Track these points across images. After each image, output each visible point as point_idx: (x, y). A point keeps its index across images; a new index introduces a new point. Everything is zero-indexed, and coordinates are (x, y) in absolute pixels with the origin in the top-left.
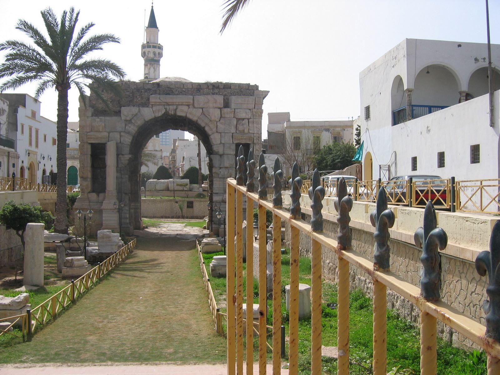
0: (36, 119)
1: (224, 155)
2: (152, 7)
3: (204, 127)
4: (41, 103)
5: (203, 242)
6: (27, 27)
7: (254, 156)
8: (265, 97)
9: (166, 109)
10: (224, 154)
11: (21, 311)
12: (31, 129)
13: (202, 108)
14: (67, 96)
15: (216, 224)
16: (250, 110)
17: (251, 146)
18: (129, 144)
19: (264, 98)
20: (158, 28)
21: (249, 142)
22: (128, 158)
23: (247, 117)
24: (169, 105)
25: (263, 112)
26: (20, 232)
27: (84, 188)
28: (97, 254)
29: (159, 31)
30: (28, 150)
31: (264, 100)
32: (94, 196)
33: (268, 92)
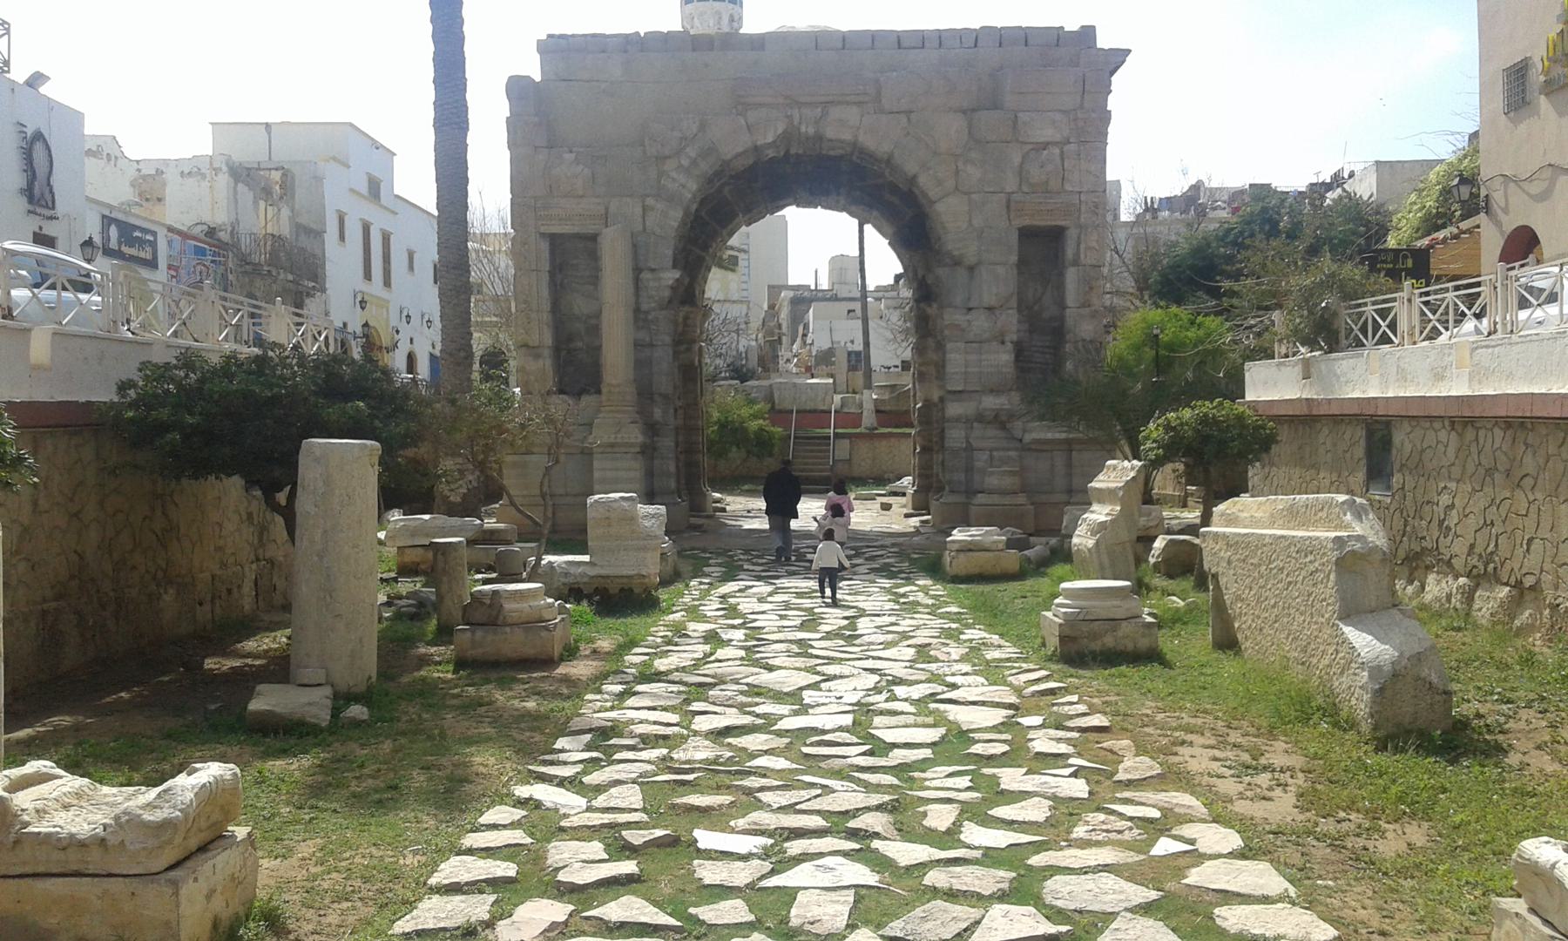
3: (915, 177)
4: (395, 154)
5: (953, 541)
7: (1071, 276)
8: (1118, 67)
9: (790, 117)
10: (979, 263)
11: (175, 884)
14: (465, 90)
15: (958, 492)
16: (1064, 112)
17: (1072, 234)
19: (1113, 73)
23: (1058, 138)
24: (800, 105)
25: (1110, 119)
26: (282, 497)
27: (532, 378)
28: (585, 580)
31: (1113, 78)
32: (560, 405)
33: (1129, 51)
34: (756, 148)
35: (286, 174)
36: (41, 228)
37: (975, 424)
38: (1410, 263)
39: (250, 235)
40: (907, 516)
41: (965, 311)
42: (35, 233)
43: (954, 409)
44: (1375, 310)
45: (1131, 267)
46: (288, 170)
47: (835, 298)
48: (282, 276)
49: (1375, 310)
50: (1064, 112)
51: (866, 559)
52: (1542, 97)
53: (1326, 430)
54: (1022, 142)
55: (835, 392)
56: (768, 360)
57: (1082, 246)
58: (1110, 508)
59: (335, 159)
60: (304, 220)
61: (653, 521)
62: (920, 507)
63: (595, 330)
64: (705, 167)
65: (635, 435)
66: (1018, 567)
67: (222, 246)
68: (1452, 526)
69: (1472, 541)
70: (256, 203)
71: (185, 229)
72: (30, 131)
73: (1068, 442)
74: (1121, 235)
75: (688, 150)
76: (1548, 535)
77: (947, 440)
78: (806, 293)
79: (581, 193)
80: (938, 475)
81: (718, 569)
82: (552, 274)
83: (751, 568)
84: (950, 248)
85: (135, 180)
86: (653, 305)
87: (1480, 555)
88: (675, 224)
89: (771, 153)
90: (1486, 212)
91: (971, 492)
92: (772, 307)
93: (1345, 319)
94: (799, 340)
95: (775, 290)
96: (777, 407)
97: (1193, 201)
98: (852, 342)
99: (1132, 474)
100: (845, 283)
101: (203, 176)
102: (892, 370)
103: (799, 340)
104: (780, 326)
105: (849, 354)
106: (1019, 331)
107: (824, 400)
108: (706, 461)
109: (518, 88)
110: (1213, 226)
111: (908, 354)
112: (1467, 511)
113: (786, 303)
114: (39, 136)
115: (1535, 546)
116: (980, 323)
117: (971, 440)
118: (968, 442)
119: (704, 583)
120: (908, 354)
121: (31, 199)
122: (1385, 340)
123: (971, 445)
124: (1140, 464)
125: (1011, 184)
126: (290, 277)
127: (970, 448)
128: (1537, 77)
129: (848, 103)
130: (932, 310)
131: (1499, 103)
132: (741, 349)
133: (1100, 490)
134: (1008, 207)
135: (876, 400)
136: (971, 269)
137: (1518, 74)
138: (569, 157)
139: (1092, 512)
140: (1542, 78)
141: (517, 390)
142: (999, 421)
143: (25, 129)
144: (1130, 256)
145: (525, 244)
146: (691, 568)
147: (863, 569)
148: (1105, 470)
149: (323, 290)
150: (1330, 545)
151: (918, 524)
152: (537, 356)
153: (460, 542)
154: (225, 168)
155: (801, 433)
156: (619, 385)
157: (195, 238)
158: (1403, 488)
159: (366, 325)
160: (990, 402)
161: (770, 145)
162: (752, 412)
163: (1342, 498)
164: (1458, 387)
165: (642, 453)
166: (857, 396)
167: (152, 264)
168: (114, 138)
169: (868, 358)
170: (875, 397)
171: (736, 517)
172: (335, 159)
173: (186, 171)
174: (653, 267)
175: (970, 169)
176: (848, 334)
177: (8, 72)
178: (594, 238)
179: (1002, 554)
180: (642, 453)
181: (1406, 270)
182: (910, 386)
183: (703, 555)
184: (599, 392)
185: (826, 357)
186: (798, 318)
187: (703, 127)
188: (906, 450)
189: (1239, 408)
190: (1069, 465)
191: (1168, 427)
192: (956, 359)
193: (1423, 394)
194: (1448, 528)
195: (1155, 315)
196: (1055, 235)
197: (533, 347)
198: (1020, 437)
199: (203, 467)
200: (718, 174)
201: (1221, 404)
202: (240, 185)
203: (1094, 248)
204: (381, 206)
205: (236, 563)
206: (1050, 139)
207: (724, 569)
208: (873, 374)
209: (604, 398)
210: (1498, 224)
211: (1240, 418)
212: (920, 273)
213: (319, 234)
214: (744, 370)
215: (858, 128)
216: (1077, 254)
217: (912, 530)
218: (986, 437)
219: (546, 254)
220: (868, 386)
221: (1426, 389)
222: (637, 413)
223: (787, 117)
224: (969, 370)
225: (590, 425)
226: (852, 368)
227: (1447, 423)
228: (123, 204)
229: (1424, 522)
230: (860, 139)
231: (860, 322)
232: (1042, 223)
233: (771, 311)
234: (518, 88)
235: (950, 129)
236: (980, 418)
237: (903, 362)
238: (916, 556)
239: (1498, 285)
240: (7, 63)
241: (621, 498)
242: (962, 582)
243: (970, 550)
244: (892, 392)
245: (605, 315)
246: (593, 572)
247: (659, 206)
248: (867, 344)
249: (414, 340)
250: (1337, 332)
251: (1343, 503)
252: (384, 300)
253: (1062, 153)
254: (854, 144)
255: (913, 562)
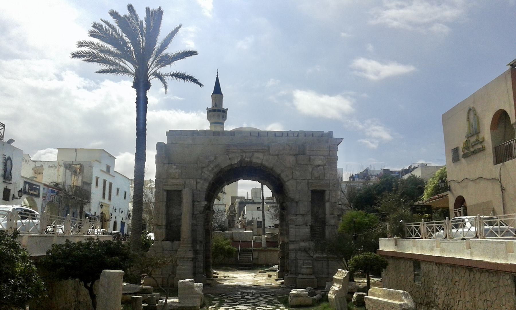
0: (111, 173)
1: (300, 202)
2: (217, 76)
5: (291, 294)
6: (114, 14)
7: (327, 205)
9: (242, 156)
12: (105, 182)
13: (278, 155)
16: (324, 156)
17: (327, 192)
18: (205, 190)
20: (222, 94)
21: (324, 189)
22: (204, 205)
23: (322, 163)
24: (245, 152)
26: (89, 285)
29: (223, 96)
30: (101, 202)
33: (343, 139)
34: (231, 165)
35: (82, 166)
36: (6, 187)
37: (298, 252)
38: (426, 209)
39: (69, 186)
40: (277, 280)
41: (295, 216)
42: (4, 188)
43: (291, 247)
44: (415, 226)
45: (347, 197)
46: (82, 165)
47: (253, 203)
48: (78, 199)
49: (415, 226)
50: (324, 156)
51: (264, 298)
52: (463, 159)
53: (402, 262)
54: (312, 165)
55: (253, 235)
56: (231, 224)
57: (331, 196)
58: (339, 285)
59: (97, 160)
60: (85, 180)
61: (199, 288)
62: (280, 277)
63: (179, 220)
64: (216, 170)
65: (191, 254)
66: (312, 303)
67: (60, 190)
68: (438, 295)
69: (443, 300)
70: (71, 175)
71: (48, 184)
72: (7, 157)
73: (327, 258)
74: (343, 186)
75: (211, 165)
76: (463, 300)
77: (289, 257)
78: (244, 200)
79: (177, 178)
80: (286, 266)
81: (217, 302)
82: (167, 202)
83: (228, 301)
84: (291, 196)
85: (34, 168)
86: (198, 212)
87: (446, 305)
88: (206, 188)
89: (236, 166)
90: (450, 191)
91: (297, 274)
92: (232, 204)
93: (406, 228)
94: (241, 216)
95: (234, 198)
96: (234, 240)
97: (365, 175)
98: (259, 218)
99: (345, 275)
100: (256, 197)
101: (56, 167)
102: (272, 227)
103: (241, 216)
104: (235, 211)
105: (258, 222)
106: (312, 222)
107: (249, 238)
108: (211, 261)
109: (160, 146)
110: (372, 184)
111: (278, 222)
112: (442, 290)
113: (237, 203)
114: (9, 158)
115: (460, 303)
116: (300, 220)
117: (297, 257)
118: (296, 257)
119: (213, 308)
120: (278, 222)
121: (4, 178)
122: (417, 236)
123: (297, 259)
124: (348, 272)
125: (309, 177)
126: (80, 199)
127: (296, 259)
128: (461, 153)
129: (260, 152)
130: (285, 213)
131: (451, 159)
132: (223, 220)
133: (336, 279)
134: (308, 184)
135: (266, 238)
136: (297, 202)
137: (455, 151)
138: (174, 167)
139: (334, 286)
140: (462, 153)
141: (152, 235)
142: (306, 250)
143: (5, 156)
144: (346, 193)
145: (159, 193)
146: (208, 301)
147: (263, 302)
148: (338, 272)
149: (90, 202)
150: (398, 306)
151: (280, 284)
152: (160, 229)
153: (140, 297)
154: (63, 165)
155: (243, 249)
156: (186, 238)
157: (51, 187)
158: (424, 282)
159: (102, 213)
160: (303, 244)
161: (236, 164)
162: (226, 243)
163: (401, 292)
164: (437, 254)
165: (192, 260)
166: (260, 237)
167: (38, 196)
168: (29, 155)
169: (264, 224)
170: (266, 237)
171: (221, 280)
172: (97, 160)
173: (50, 166)
174: (199, 200)
175: (297, 172)
176: (257, 215)
177: (3, 139)
178: (180, 191)
179: (306, 298)
180: (192, 260)
181: (425, 211)
182: (278, 233)
183: (211, 296)
184: (180, 240)
185: (250, 223)
186: (241, 209)
187: (216, 158)
188: (275, 255)
189: (377, 255)
190: (328, 265)
191: (356, 261)
192: (292, 231)
193: (428, 254)
194: (437, 295)
195: (354, 213)
196: (323, 192)
197: (159, 225)
198: (312, 256)
199: (65, 276)
200: (220, 172)
201: (371, 254)
202: (68, 171)
203: (334, 197)
204: (111, 175)
205: (70, 303)
206: (320, 164)
207: (219, 302)
208: (265, 229)
209: (181, 242)
210: (453, 194)
211: (377, 258)
212: (281, 201)
213: (89, 184)
214: (224, 227)
215: (263, 160)
216: (329, 199)
217: (278, 286)
218: (301, 255)
219: (165, 196)
220: (264, 234)
221: (428, 253)
222: (192, 247)
223: (241, 156)
224: (297, 234)
225: (177, 251)
226: (259, 227)
227: (435, 264)
228: (31, 177)
229: (430, 293)
230: (263, 162)
231: (262, 212)
232: (318, 189)
233: (232, 205)
234: (160, 146)
235: (290, 160)
236: (300, 250)
237: (275, 225)
238: (280, 297)
239: (447, 224)
240: (3, 136)
241: (189, 281)
242: (294, 308)
243: (297, 297)
244: (271, 235)
245: (183, 216)
246: (179, 305)
247: (202, 182)
248: (264, 220)
249: (117, 217)
250: (404, 232)
251: (402, 293)
252: (108, 205)
253: (324, 168)
254: (262, 164)
255: (279, 299)
